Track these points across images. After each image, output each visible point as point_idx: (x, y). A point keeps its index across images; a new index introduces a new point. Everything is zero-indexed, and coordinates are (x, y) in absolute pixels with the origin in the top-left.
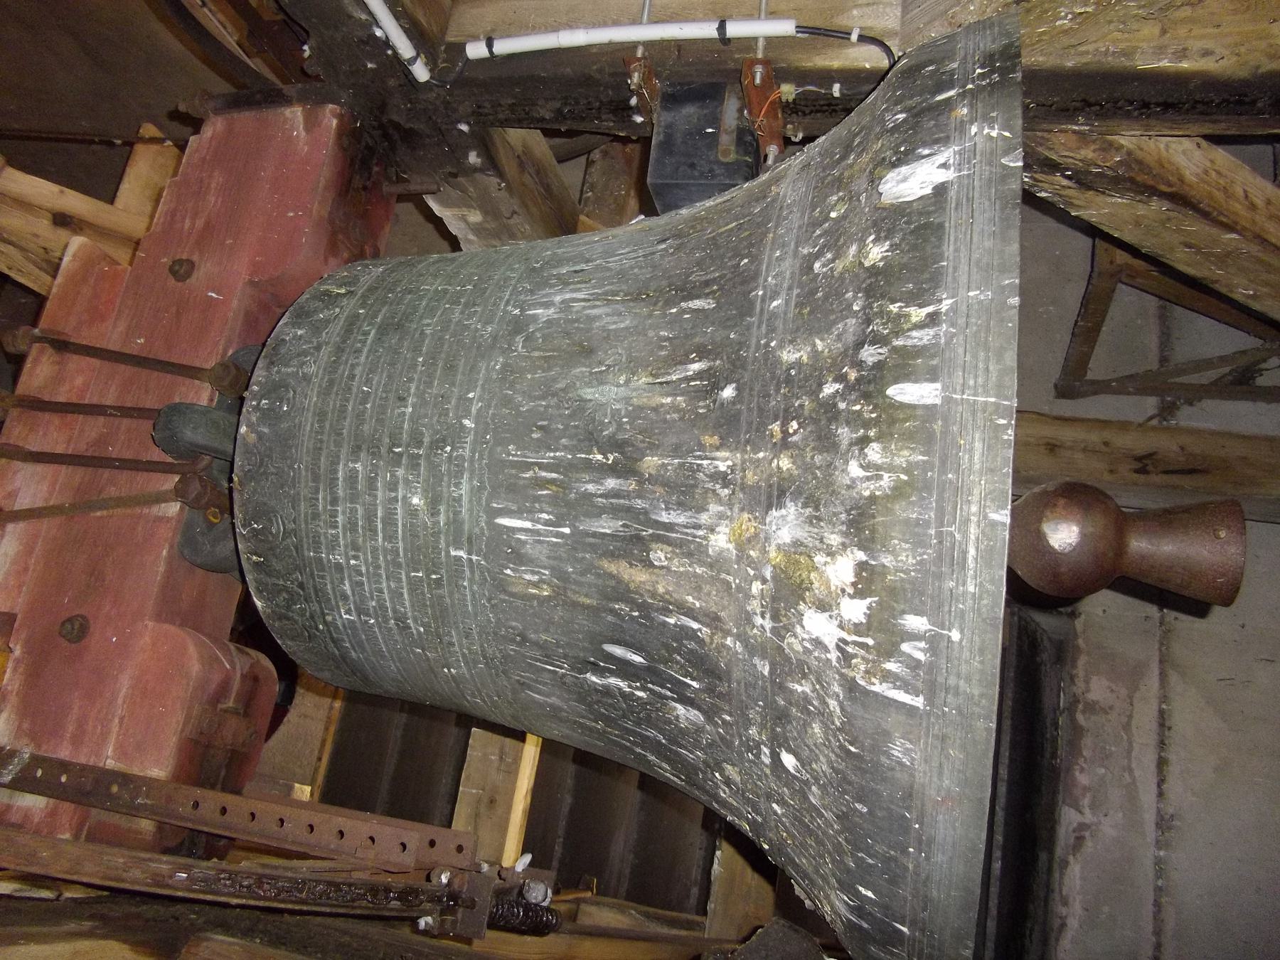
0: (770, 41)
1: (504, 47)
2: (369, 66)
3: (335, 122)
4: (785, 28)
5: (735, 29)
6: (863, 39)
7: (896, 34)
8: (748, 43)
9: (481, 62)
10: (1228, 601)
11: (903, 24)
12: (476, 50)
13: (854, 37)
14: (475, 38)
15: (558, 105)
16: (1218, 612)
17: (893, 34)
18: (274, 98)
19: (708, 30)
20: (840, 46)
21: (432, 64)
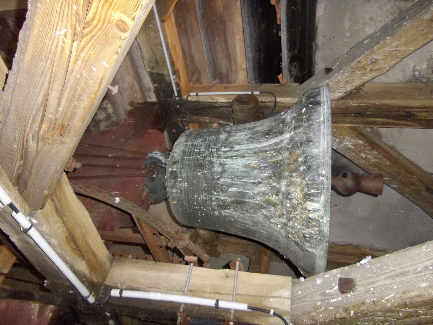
0: (237, 311)
1: (127, 294)
2: (71, 292)
3: (51, 315)
4: (243, 307)
5: (222, 304)
6: (275, 314)
7: (288, 313)
8: (227, 310)
9: (115, 298)
10: (381, 194)
11: (291, 308)
12: (115, 293)
13: (272, 313)
14: (116, 288)
15: (147, 316)
16: (379, 196)
17: (287, 313)
18: (29, 297)
19: (211, 303)
20: (265, 316)
21: (97, 295)
